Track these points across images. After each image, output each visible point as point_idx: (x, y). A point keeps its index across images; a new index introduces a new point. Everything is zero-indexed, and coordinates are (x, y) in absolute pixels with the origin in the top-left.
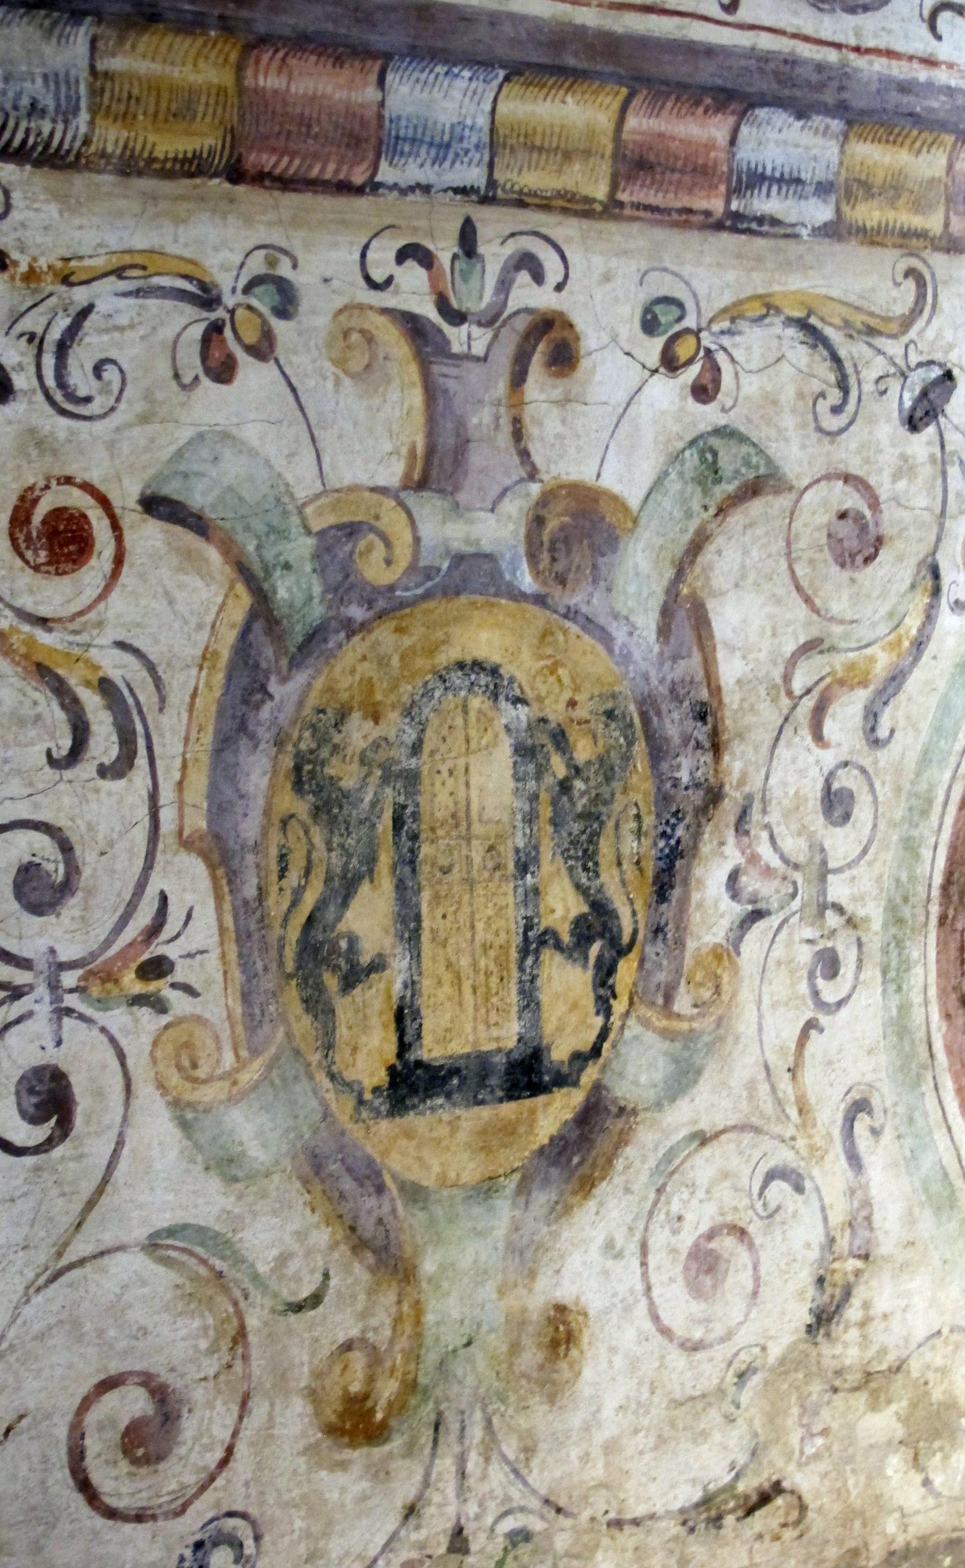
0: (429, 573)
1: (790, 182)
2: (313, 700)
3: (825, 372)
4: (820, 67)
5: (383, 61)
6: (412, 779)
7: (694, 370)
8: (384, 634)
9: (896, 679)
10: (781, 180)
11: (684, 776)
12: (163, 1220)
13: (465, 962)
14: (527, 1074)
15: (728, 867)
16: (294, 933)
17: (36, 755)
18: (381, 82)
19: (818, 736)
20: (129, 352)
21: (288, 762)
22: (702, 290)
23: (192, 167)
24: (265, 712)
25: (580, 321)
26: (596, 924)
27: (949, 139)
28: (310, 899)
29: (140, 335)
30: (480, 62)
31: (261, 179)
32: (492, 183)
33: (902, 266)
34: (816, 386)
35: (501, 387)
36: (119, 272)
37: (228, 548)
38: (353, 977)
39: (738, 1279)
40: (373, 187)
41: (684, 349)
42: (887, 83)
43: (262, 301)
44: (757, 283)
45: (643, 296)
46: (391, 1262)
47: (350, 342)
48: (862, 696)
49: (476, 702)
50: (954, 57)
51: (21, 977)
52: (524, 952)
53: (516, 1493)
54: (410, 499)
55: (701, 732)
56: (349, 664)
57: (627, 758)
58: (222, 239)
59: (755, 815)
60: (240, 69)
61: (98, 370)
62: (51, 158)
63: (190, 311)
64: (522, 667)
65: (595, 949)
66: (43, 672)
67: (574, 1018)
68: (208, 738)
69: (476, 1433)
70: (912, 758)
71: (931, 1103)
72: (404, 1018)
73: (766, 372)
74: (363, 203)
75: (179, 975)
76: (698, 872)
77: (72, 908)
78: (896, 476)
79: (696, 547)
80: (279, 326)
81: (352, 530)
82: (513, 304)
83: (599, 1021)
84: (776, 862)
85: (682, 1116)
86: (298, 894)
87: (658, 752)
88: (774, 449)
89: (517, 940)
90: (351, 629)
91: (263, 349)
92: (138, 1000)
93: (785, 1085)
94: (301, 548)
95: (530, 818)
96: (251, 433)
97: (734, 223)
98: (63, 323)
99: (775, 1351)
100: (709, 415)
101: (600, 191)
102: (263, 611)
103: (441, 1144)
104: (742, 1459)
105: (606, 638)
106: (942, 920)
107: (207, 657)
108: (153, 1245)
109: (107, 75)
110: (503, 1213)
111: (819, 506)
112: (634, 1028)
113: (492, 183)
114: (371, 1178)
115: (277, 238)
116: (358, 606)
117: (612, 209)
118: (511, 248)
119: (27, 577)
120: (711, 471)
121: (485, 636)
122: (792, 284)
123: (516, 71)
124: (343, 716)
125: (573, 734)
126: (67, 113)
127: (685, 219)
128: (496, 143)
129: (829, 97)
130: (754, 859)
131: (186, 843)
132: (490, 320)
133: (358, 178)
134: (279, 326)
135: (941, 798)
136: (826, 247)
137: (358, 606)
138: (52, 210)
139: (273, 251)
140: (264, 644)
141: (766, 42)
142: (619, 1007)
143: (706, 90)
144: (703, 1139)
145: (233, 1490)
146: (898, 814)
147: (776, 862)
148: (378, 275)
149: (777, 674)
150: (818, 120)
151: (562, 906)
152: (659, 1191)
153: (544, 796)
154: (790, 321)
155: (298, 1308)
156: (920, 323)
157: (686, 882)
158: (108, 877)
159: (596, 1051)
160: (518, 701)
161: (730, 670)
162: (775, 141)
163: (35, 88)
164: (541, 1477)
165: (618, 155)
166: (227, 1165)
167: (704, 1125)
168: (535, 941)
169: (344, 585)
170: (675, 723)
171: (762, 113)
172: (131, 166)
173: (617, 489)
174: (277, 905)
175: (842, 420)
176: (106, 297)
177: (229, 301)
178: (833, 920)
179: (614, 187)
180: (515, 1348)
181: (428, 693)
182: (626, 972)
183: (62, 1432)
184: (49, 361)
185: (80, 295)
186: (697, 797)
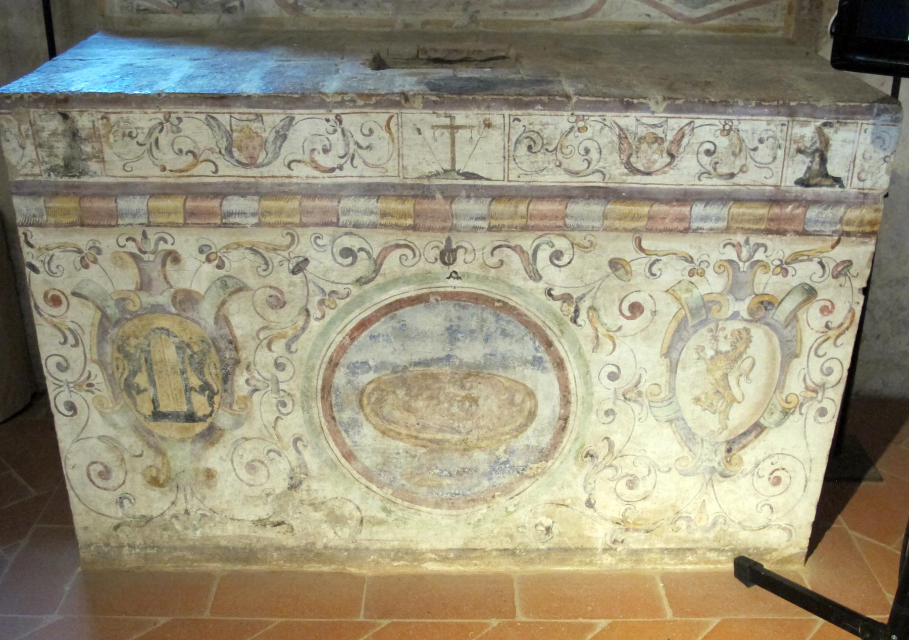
0: (145, 309)
1: (242, 214)
2: (120, 333)
3: (259, 260)
4: (248, 183)
5: (116, 197)
6: (149, 352)
7: (216, 262)
8: (136, 321)
9: (296, 337)
10: (239, 213)
11: (228, 356)
12: (101, 434)
13: (169, 392)
14: (191, 417)
15: (245, 378)
16: (122, 381)
17: (57, 341)
18: (116, 202)
19: (270, 350)
20: (63, 263)
21: (115, 347)
22: (216, 243)
23: (72, 225)
24: (109, 336)
25: (179, 251)
26: (205, 388)
27: (299, 197)
28: (125, 376)
29: (66, 260)
30: (142, 194)
31: (89, 225)
32: (149, 222)
33: (286, 231)
34: (257, 264)
35: (159, 267)
36: (59, 247)
37: (93, 302)
38: (140, 392)
39: (263, 472)
40: (117, 225)
41: (212, 257)
42: (273, 185)
43: (93, 252)
44: (234, 239)
45: (199, 244)
46: (159, 452)
47: (116, 259)
48: (284, 341)
49: (164, 337)
50: (299, 174)
51: (61, 384)
52: (186, 391)
53: (202, 506)
54: (138, 293)
55: (231, 347)
56: (128, 327)
57: (209, 351)
58: (82, 239)
59: (252, 367)
60: (80, 203)
61: (57, 267)
62: (40, 225)
63: (77, 255)
64: (175, 329)
65: (207, 393)
66: (55, 326)
67: (203, 407)
68: (95, 341)
69: (189, 491)
70: (305, 357)
71: (324, 442)
72: (154, 401)
73: (239, 263)
74: (116, 229)
75: (96, 386)
76: (236, 378)
77: (69, 372)
78: (289, 286)
79: (223, 303)
80: (98, 257)
81: (124, 299)
82: (160, 248)
83: (210, 409)
84: (261, 378)
85: (239, 433)
86: (122, 374)
87: (218, 350)
88: (244, 280)
89: (183, 388)
90: (127, 320)
91: (95, 261)
92: (87, 391)
93: (272, 430)
94: (111, 303)
95: (183, 362)
96: (95, 279)
97: (225, 225)
98: (48, 258)
99: (278, 491)
100: (222, 273)
101: (181, 221)
102: (104, 315)
103: (168, 430)
104: (271, 513)
105: (198, 323)
106: (322, 398)
107: (92, 325)
108: (99, 438)
109: (49, 208)
110: (188, 447)
111: (262, 295)
112: (220, 412)
113: (149, 222)
114: (150, 433)
115: (94, 238)
116: (126, 315)
117: (185, 225)
118: (157, 236)
119: (49, 308)
120: (225, 286)
121: (164, 323)
122: (245, 239)
123: (152, 196)
124: (128, 338)
125: (192, 345)
126: (42, 216)
127: (208, 226)
128: (149, 212)
129: (253, 191)
130: (253, 377)
131: (94, 361)
132: (153, 253)
133: (113, 223)
134: (98, 257)
135: (318, 367)
136: (255, 229)
137: (126, 315)
138: (41, 236)
139: (94, 241)
140: (105, 324)
141: (228, 179)
142: (216, 406)
143: (211, 194)
144: (246, 439)
145: (127, 488)
146: (302, 370)
147: (261, 378)
148: (121, 244)
149: (254, 334)
150: (249, 197)
151: (195, 382)
152: (235, 449)
153: (186, 358)
154: (247, 248)
155: (137, 456)
156: (293, 247)
157: (232, 380)
158: (77, 365)
159: (210, 415)
160: (175, 337)
161: (238, 333)
162: (234, 204)
163: (33, 212)
164: (209, 503)
165: (185, 211)
166: (115, 426)
167: (246, 436)
168: (188, 389)
169: (124, 310)
170: (223, 344)
171: (229, 198)
172: (57, 225)
173: (197, 290)
174: (117, 375)
175: (267, 273)
176: (56, 252)
177: (85, 252)
178: (282, 393)
179: (185, 219)
180: (197, 475)
181: (150, 334)
182: (217, 399)
183: (85, 470)
184: (46, 266)
185: (51, 252)
186: (233, 361)
